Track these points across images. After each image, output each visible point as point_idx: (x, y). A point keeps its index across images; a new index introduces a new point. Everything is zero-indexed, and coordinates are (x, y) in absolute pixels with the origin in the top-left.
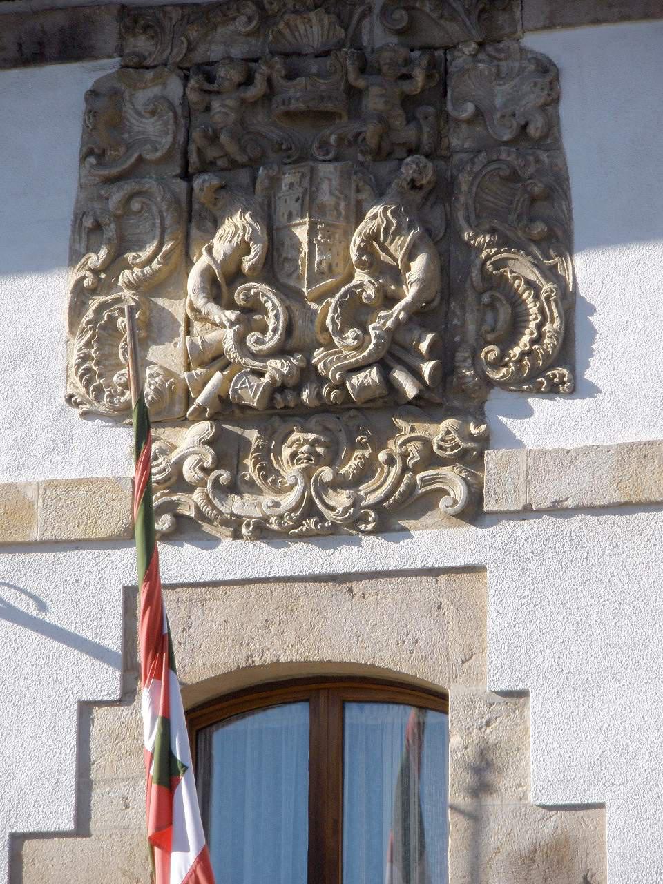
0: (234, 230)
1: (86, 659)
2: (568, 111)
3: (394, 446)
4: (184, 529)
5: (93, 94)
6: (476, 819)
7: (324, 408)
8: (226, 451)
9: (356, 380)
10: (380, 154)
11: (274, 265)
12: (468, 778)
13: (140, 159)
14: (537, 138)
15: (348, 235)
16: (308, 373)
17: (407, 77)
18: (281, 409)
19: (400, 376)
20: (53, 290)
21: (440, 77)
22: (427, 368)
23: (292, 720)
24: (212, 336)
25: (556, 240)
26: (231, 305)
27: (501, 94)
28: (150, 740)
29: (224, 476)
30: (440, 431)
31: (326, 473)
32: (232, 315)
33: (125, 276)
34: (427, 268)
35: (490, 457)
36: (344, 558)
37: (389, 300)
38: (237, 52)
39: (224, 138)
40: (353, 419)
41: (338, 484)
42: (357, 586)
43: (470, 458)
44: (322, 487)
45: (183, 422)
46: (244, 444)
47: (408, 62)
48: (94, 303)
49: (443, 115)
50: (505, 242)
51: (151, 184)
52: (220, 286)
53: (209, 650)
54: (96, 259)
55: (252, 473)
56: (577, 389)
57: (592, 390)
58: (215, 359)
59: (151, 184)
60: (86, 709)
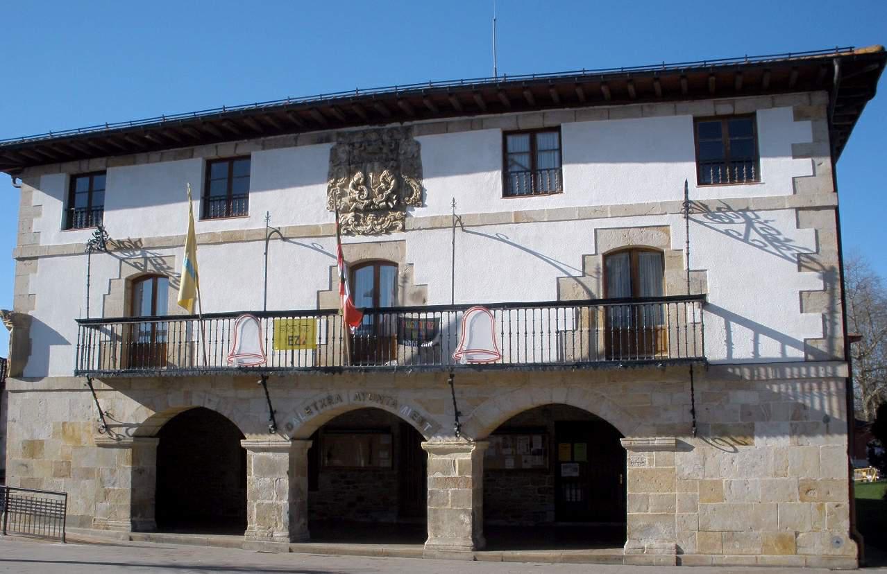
0: (358, 176)
1: (331, 258)
2: (422, 152)
3: (389, 217)
4: (349, 233)
5: (331, 150)
6: (403, 287)
7: (375, 210)
8: (357, 218)
9: (381, 204)
10: (386, 161)
11: (366, 182)
12: (402, 280)
13: (341, 162)
14: (416, 157)
15: (379, 178)
16: (372, 203)
17: (391, 146)
18: (367, 210)
19: (389, 203)
20: (323, 188)
21: (397, 145)
22: (395, 202)
23: (371, 269)
24: (354, 196)
25: (419, 177)
26: (357, 190)
27: (409, 148)
28: (340, 274)
29: (356, 223)
30: (397, 214)
31: (376, 222)
32: (358, 192)
33: (338, 184)
34: (395, 183)
35: (407, 219)
36: (379, 238)
37: (387, 189)
38: (359, 140)
39: (356, 158)
40: (381, 212)
41: (378, 224)
42: (382, 244)
43: (403, 220)
44: (375, 225)
45: (349, 212)
46: (360, 216)
47: (391, 143)
48: (332, 190)
49: (398, 153)
50: (410, 177)
51: (342, 166)
52: (355, 187)
53: (352, 257)
54: (332, 181)
55: (362, 222)
56: (423, 206)
57: (426, 206)
58: (354, 200)
59: (342, 166)
60: (331, 267)
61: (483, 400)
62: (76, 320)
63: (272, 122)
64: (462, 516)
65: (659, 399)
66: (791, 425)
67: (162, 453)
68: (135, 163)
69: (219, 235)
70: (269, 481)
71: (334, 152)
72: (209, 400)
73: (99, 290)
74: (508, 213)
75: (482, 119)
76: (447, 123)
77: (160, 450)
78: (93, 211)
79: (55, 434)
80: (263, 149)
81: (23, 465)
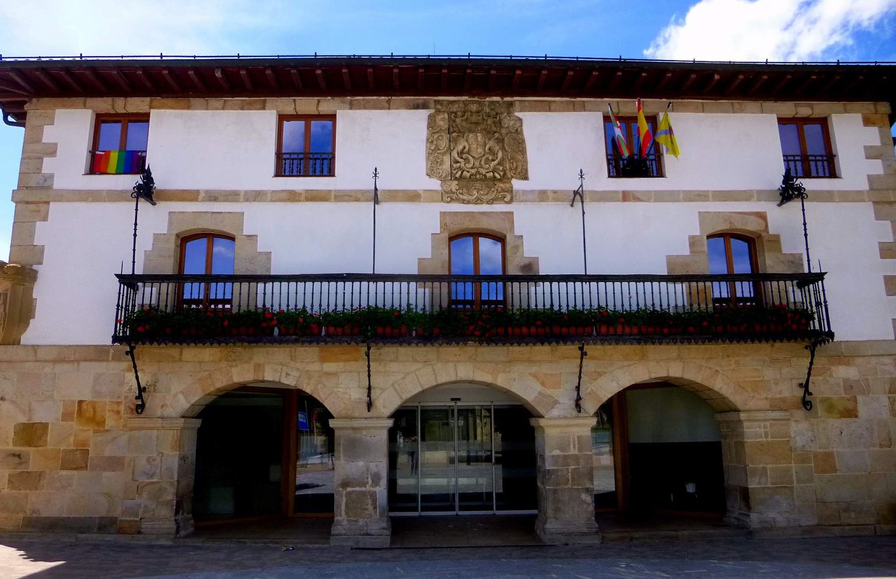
2: (525, 127)
16: (478, 172)
27: (512, 123)
61: (600, 374)
62: (117, 275)
63: (47, 81)
64: (584, 496)
65: (769, 374)
66: (889, 398)
67: (202, 434)
68: (189, 108)
69: (300, 194)
70: (456, 461)
71: (431, 122)
72: (287, 374)
73: (145, 243)
74: (616, 192)
75: (584, 102)
76: (550, 102)
77: (201, 432)
78: (285, 159)
79: (66, 416)
80: (351, 109)
81: (14, 455)
